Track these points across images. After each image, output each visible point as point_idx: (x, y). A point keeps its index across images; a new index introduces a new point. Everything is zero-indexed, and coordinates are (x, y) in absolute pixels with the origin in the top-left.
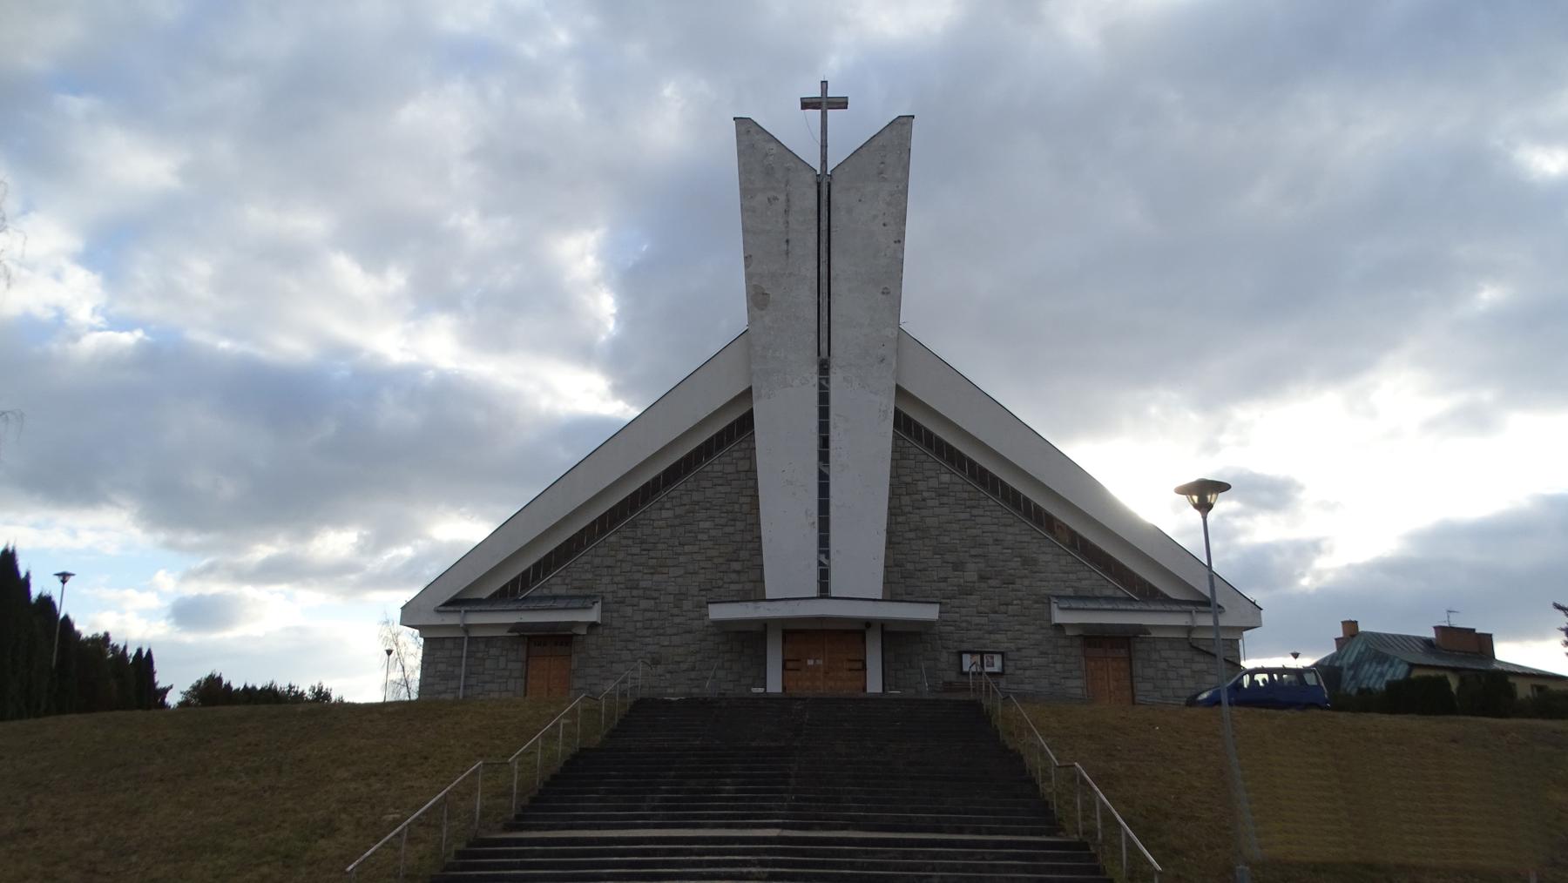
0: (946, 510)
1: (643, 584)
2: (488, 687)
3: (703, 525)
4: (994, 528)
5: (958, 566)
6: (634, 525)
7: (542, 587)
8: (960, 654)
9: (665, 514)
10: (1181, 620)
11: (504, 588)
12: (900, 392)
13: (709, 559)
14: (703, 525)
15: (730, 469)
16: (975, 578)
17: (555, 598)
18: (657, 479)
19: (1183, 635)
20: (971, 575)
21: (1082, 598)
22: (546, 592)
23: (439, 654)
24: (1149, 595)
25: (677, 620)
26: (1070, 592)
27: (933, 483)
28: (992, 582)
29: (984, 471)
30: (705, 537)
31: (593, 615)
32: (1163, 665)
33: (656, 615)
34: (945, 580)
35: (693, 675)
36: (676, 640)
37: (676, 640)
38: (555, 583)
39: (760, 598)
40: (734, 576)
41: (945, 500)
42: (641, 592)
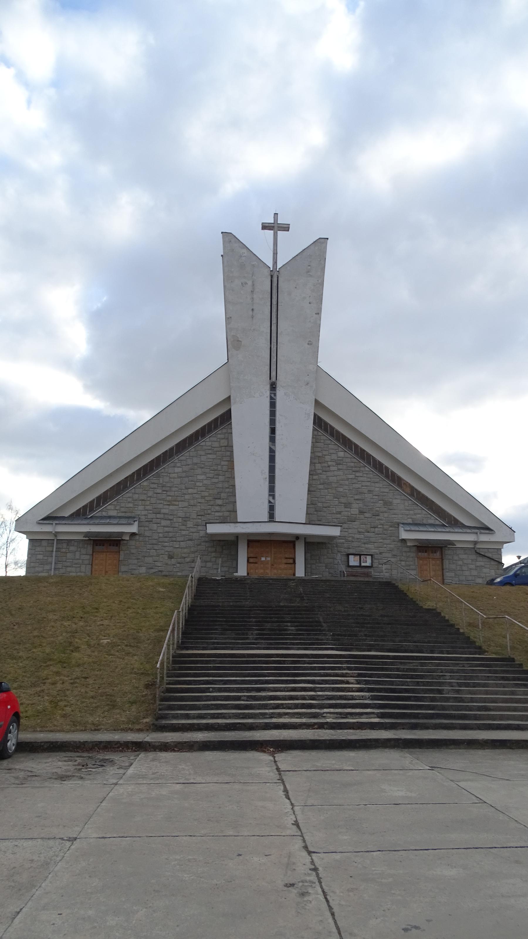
0: (340, 473)
1: (163, 511)
3: (200, 477)
4: (368, 484)
5: (348, 505)
6: (158, 476)
9: (177, 470)
10: (471, 538)
12: (317, 403)
13: (203, 497)
15: (216, 444)
16: (357, 512)
19: (472, 546)
20: (354, 510)
22: (104, 514)
24: (454, 523)
25: (184, 533)
26: (410, 521)
27: (334, 457)
28: (367, 515)
29: (363, 451)
30: (201, 484)
31: (134, 529)
33: (171, 529)
34: (340, 513)
38: (110, 509)
40: (217, 508)
41: (340, 467)
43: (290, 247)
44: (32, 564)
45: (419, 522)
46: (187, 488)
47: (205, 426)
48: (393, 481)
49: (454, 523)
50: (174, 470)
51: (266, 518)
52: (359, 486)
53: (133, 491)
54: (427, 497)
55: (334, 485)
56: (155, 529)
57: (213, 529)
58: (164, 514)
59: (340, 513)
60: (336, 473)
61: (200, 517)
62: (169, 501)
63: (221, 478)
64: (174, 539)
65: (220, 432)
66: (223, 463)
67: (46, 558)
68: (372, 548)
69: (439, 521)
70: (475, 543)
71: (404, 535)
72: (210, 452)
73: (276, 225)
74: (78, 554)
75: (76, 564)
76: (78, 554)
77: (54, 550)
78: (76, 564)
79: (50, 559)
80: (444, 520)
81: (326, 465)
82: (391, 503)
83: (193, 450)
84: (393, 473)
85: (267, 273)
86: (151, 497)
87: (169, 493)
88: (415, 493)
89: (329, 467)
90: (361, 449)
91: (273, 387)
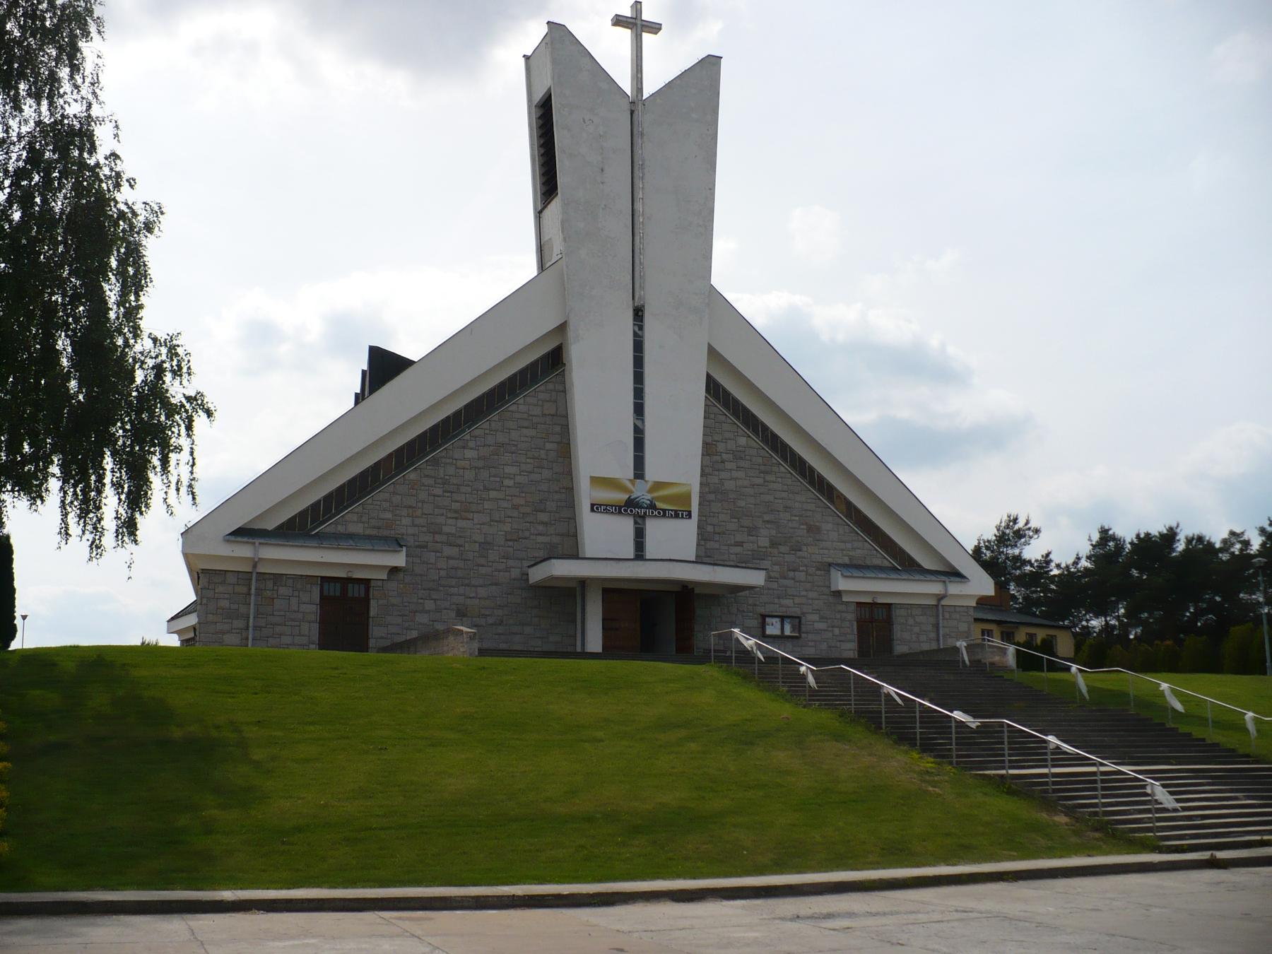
0: (741, 474)
1: (445, 529)
2: (278, 629)
3: (508, 470)
4: (784, 495)
5: (752, 531)
6: (435, 462)
7: (336, 523)
8: (764, 617)
9: (469, 454)
10: (934, 588)
11: (291, 521)
12: (713, 353)
13: (516, 507)
14: (508, 470)
15: (537, 411)
16: (767, 544)
17: (351, 536)
18: (457, 414)
19: (934, 602)
20: (764, 542)
21: (856, 567)
22: (341, 529)
23: (220, 589)
24: (907, 566)
25: (483, 570)
26: (847, 560)
27: (731, 445)
28: (782, 549)
29: (775, 437)
30: (510, 483)
31: (399, 560)
32: (916, 629)
33: (461, 564)
34: (740, 544)
35: (501, 629)
36: (483, 592)
37: (483, 592)
38: (350, 519)
39: (574, 554)
40: (541, 528)
41: (742, 463)
42: (444, 538)
43: (664, 64)
44: (210, 617)
45: (860, 562)
46: (486, 489)
47: (515, 375)
48: (821, 491)
49: (907, 566)
50: (464, 453)
51: (630, 553)
52: (770, 498)
53: (391, 489)
54: (878, 528)
55: (732, 496)
56: (433, 561)
57: (538, 574)
58: (447, 534)
59: (740, 544)
60: (735, 474)
61: (510, 543)
62: (456, 512)
63: (546, 473)
64: (467, 582)
65: (542, 388)
66: (549, 446)
67: (236, 606)
68: (790, 606)
69: (888, 561)
70: (940, 598)
71: (842, 583)
72: (526, 424)
73: (639, 22)
74: (294, 601)
75: (293, 620)
76: (294, 601)
77: (253, 591)
78: (293, 620)
79: (243, 610)
80: (894, 558)
81: (718, 458)
82: (818, 529)
83: (496, 418)
84: (821, 478)
85: (627, 107)
86: (423, 502)
87: (456, 497)
88: (852, 512)
89: (723, 462)
90: (772, 433)
91: (638, 314)
